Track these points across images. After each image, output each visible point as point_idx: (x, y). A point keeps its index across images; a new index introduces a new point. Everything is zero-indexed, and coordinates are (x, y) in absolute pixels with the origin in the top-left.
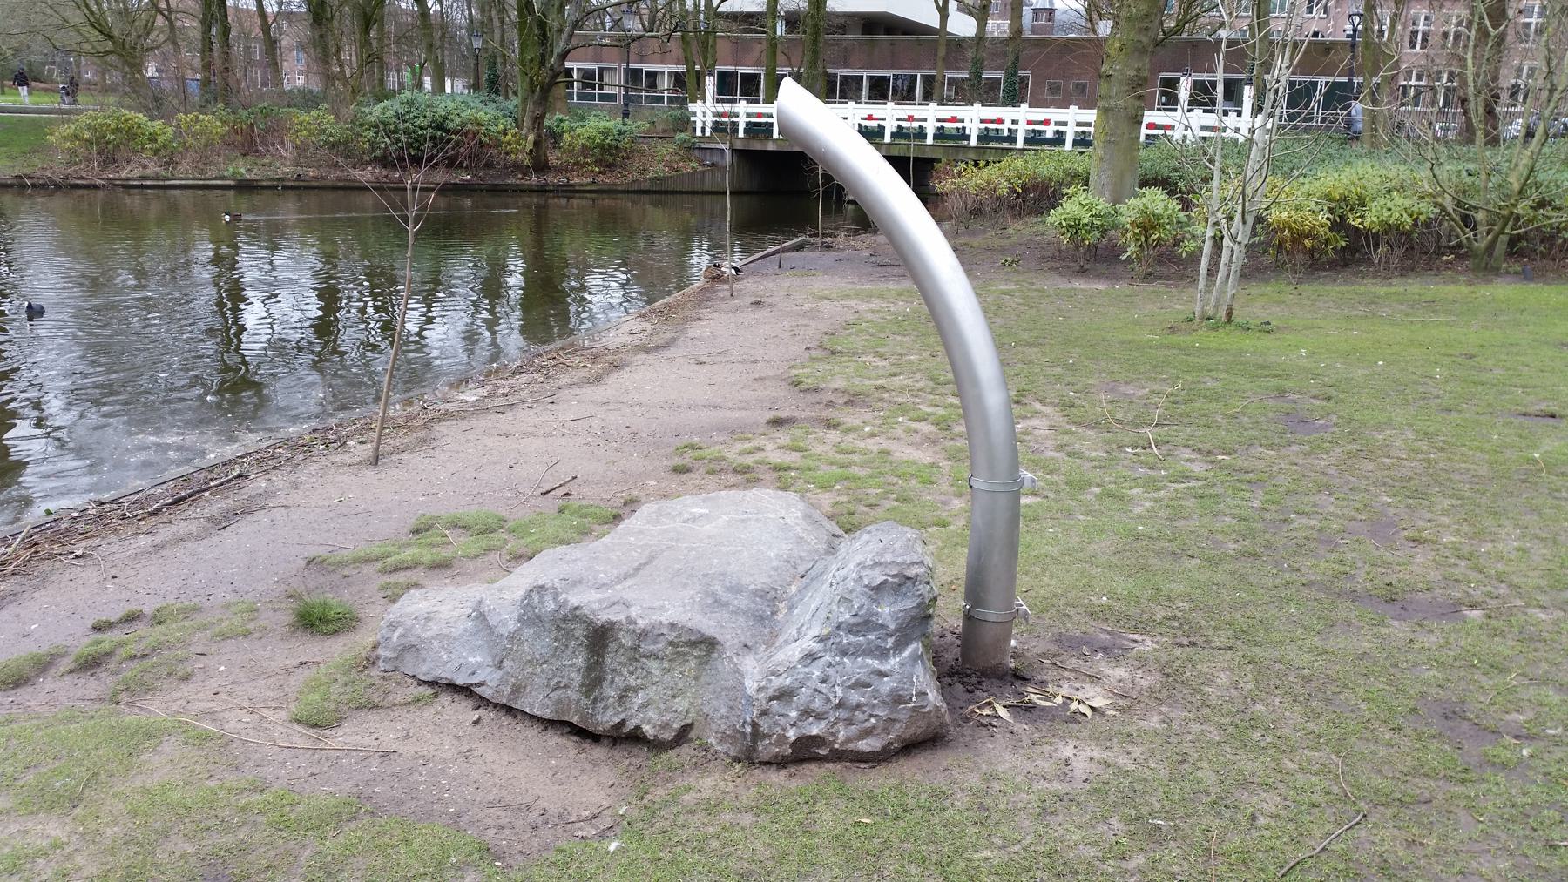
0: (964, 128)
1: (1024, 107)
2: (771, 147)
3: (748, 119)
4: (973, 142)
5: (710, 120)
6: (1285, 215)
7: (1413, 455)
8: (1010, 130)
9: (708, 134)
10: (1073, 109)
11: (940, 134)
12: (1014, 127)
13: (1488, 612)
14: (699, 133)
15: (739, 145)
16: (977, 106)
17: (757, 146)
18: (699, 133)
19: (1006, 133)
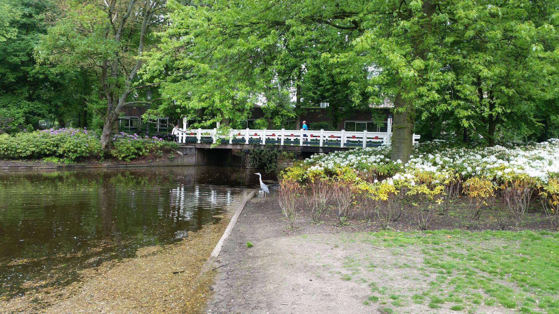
0: (260, 138)
1: (365, 132)
2: (212, 146)
3: (202, 136)
4: (264, 143)
5: (185, 136)
6: (380, 40)
7: (334, 90)
8: (278, 138)
9: (184, 141)
10: (365, 132)
11: (251, 140)
12: (279, 138)
13: (428, 257)
14: (180, 141)
15: (198, 147)
16: (283, 130)
17: (207, 146)
18: (180, 141)
19: (276, 140)
